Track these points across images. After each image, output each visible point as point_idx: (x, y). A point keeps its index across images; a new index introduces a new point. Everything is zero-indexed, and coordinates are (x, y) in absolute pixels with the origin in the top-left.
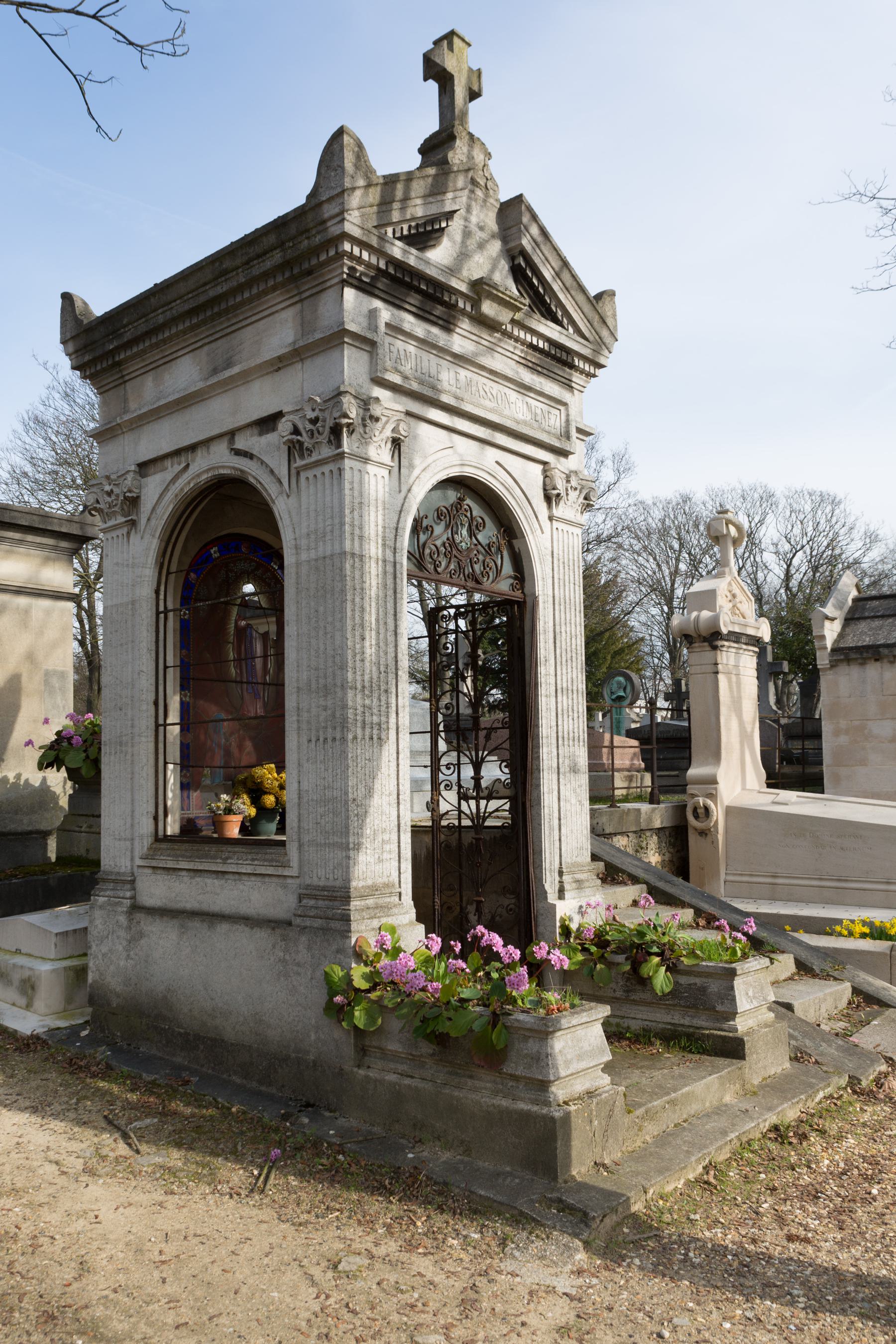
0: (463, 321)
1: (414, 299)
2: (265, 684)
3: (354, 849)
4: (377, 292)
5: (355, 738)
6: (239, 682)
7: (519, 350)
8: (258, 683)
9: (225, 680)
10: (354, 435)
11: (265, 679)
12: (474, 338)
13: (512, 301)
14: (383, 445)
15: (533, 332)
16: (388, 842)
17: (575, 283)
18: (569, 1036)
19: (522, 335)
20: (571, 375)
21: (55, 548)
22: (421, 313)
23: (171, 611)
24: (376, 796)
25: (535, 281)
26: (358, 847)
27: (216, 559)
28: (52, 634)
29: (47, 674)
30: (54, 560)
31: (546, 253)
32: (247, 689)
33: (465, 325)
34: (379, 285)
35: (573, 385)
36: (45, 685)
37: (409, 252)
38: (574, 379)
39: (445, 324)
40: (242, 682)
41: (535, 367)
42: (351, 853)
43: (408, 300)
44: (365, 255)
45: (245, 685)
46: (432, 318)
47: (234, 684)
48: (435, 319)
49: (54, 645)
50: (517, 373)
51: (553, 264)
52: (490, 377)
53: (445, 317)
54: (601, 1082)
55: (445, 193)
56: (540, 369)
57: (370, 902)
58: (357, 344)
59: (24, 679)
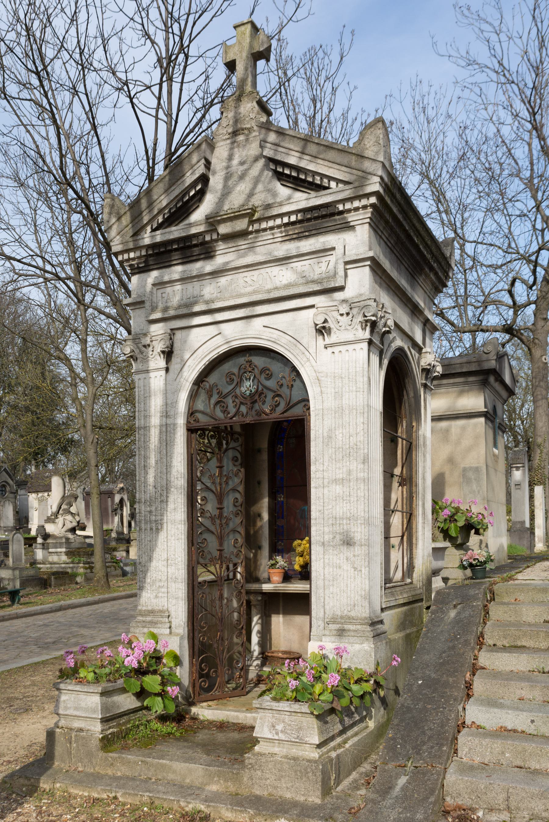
1: (176, 256)
4: (151, 267)
7: (278, 233)
12: (233, 249)
15: (281, 216)
16: (162, 587)
17: (322, 148)
20: (345, 218)
21: (466, 383)
22: (185, 260)
24: (154, 561)
25: (287, 172)
28: (466, 442)
29: (465, 470)
30: (468, 391)
31: (286, 145)
33: (221, 246)
34: (151, 263)
35: (352, 224)
36: (463, 478)
38: (349, 220)
39: (207, 255)
41: (301, 235)
44: (132, 255)
46: (195, 258)
49: (469, 449)
50: (538, 159)
51: (296, 149)
54: (93, 728)
55: (184, 176)
56: (307, 234)
57: (149, 619)
58: (138, 307)
59: (447, 476)
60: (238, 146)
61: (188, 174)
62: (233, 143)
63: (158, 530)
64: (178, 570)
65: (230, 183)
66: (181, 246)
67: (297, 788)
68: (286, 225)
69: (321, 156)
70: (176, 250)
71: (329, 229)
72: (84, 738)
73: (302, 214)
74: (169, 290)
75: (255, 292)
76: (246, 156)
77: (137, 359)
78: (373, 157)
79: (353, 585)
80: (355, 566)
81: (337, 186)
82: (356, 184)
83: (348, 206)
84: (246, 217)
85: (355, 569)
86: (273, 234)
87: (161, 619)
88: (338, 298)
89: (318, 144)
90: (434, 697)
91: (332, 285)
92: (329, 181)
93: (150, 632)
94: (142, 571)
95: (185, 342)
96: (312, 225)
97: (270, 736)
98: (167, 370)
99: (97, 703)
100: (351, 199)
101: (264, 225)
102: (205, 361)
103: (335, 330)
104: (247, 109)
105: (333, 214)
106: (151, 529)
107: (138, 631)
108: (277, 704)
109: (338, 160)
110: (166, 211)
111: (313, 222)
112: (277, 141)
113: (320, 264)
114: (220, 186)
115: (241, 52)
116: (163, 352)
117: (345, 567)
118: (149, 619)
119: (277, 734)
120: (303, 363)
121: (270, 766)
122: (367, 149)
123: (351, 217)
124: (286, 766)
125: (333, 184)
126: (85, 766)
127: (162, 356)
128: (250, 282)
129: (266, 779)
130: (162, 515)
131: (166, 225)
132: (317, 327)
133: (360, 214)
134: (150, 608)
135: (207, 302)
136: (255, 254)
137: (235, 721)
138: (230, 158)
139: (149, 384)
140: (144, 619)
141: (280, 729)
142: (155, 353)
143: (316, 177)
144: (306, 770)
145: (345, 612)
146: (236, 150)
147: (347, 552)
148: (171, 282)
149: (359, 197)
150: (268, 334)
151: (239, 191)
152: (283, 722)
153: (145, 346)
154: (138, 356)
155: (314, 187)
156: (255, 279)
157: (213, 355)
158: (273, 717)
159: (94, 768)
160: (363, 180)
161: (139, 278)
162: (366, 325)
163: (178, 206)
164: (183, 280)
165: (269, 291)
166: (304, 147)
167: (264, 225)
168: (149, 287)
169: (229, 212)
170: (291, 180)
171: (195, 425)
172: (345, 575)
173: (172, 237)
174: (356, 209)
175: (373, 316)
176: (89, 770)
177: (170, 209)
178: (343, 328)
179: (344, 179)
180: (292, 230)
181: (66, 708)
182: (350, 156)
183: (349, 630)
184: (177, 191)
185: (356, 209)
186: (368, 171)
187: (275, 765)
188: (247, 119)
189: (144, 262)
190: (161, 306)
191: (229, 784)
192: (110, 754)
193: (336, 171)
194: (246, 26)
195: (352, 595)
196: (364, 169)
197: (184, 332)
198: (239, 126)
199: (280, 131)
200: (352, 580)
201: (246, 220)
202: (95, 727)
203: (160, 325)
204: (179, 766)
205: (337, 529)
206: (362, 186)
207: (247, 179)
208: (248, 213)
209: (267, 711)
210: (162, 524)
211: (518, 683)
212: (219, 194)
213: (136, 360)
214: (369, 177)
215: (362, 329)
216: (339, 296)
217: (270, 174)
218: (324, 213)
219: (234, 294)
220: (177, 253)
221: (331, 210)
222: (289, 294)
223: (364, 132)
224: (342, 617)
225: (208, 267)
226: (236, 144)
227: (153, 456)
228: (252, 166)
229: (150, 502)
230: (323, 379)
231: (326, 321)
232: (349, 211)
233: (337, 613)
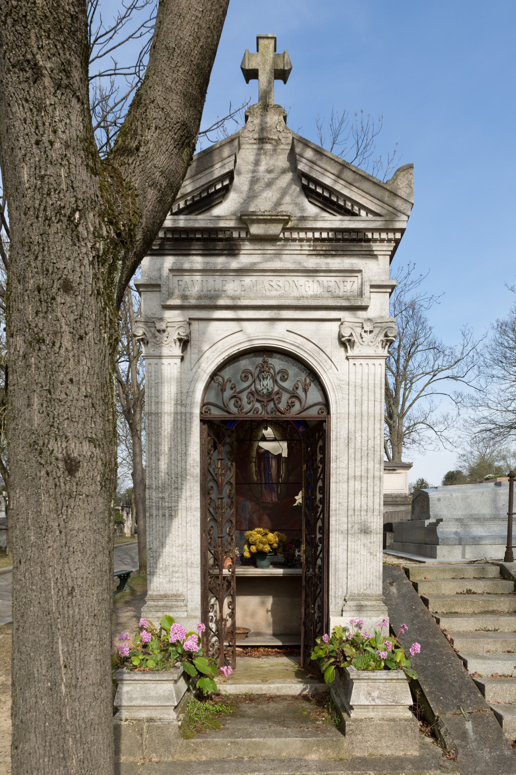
0: (244, 245)
1: (197, 245)
2: (278, 483)
3: (150, 575)
4: (167, 252)
5: (151, 515)
7: (306, 246)
8: (273, 483)
10: (149, 345)
11: (278, 480)
12: (259, 252)
13: (273, 217)
14: (173, 345)
15: (313, 230)
17: (358, 177)
18: (138, 685)
19: (302, 235)
20: (370, 246)
22: (206, 252)
25: (319, 190)
26: (153, 574)
31: (323, 165)
33: (247, 246)
34: (167, 247)
35: (375, 253)
37: (178, 220)
38: (374, 249)
39: (230, 252)
40: (261, 484)
41: (328, 253)
42: (148, 577)
43: (192, 248)
46: (217, 252)
47: (256, 485)
48: (220, 252)
51: (332, 171)
52: (275, 274)
53: (228, 248)
54: (166, 716)
55: (212, 166)
56: (334, 253)
57: (161, 603)
58: (150, 290)
60: (265, 154)
61: (217, 166)
62: (260, 149)
63: (171, 517)
64: (194, 555)
65: (256, 187)
66: (205, 236)
67: (396, 745)
68: (316, 240)
69: (356, 184)
70: (198, 240)
71: (354, 253)
72: (159, 727)
73: (333, 233)
74: (187, 278)
75: (280, 297)
76: (274, 165)
77: (148, 343)
78: (405, 198)
79: (369, 568)
80: (371, 551)
81: (367, 215)
82: (387, 218)
83: (376, 236)
84: (281, 223)
85: (371, 554)
86: (301, 246)
87: (176, 603)
88: (361, 317)
89: (354, 172)
90: (435, 655)
91: (359, 303)
92: (359, 210)
93: (166, 616)
94: (153, 557)
95: (204, 333)
96: (340, 246)
97: (367, 703)
98: (182, 359)
99: (171, 691)
100: (379, 230)
101: (295, 235)
102: (225, 355)
103: (358, 344)
104: (273, 120)
105: (361, 240)
106: (164, 515)
107: (150, 616)
108: (374, 674)
109: (373, 192)
110: (189, 198)
111: (341, 243)
112: (314, 159)
113: (345, 283)
114: (245, 188)
115: (264, 64)
116: (180, 340)
117: (362, 553)
118: (161, 603)
119: (374, 700)
120: (326, 370)
121: (370, 730)
122: (400, 189)
123: (376, 247)
124: (386, 728)
125: (363, 213)
126: (161, 756)
127: (178, 343)
128: (275, 287)
129: (366, 742)
130: (177, 502)
131: (186, 212)
132: (343, 339)
133: (384, 246)
134: (162, 593)
135: (233, 298)
136: (281, 260)
137: (259, 693)
138: (257, 163)
139: (161, 370)
140: (156, 603)
141: (376, 696)
142: (169, 340)
143: (347, 203)
144: (405, 728)
145: (362, 591)
146: (263, 157)
147: (364, 539)
148: (191, 271)
149: (387, 230)
150: (291, 338)
151: (266, 198)
152: (379, 689)
153: (159, 331)
154: (150, 340)
155: (342, 212)
156: (281, 284)
157: (234, 350)
158: (368, 685)
159: (173, 756)
160: (393, 216)
161: (151, 261)
162: (386, 344)
163: (203, 196)
164: (204, 271)
165: (298, 298)
166: (341, 172)
167: (295, 235)
168: (165, 272)
169: (266, 213)
170: (321, 200)
171: (207, 416)
172: (362, 559)
173: (197, 225)
174: (382, 241)
175: (394, 337)
176: (166, 759)
177: (193, 198)
178: (366, 343)
179: (375, 211)
180: (320, 247)
181: (131, 699)
182: (384, 191)
183: (366, 606)
184: (203, 181)
185: (382, 241)
186: (398, 209)
187: (376, 728)
188: (274, 130)
189: (159, 245)
190: (177, 292)
191: (329, 751)
192: (193, 740)
193: (368, 201)
194: (270, 40)
195: (368, 576)
196: (396, 206)
197: (202, 324)
198: (265, 135)
199: (318, 149)
200: (368, 563)
201: (280, 226)
202: (169, 715)
203: (177, 312)
204: (274, 742)
205: (357, 519)
206: (392, 221)
207: (274, 188)
208: (285, 220)
209: (362, 681)
210: (176, 511)
211: (485, 640)
212: (244, 195)
213: (146, 343)
214: (399, 214)
215: (382, 347)
216: (361, 314)
217: (298, 189)
218: (354, 237)
219: (260, 295)
220: (199, 243)
221: (361, 236)
222: (318, 304)
223: (397, 173)
224: (359, 595)
225: (234, 264)
226: (262, 151)
227: (166, 443)
228: (279, 176)
229: (163, 488)
230: (344, 386)
231: (351, 335)
232: (375, 240)
233: (354, 591)
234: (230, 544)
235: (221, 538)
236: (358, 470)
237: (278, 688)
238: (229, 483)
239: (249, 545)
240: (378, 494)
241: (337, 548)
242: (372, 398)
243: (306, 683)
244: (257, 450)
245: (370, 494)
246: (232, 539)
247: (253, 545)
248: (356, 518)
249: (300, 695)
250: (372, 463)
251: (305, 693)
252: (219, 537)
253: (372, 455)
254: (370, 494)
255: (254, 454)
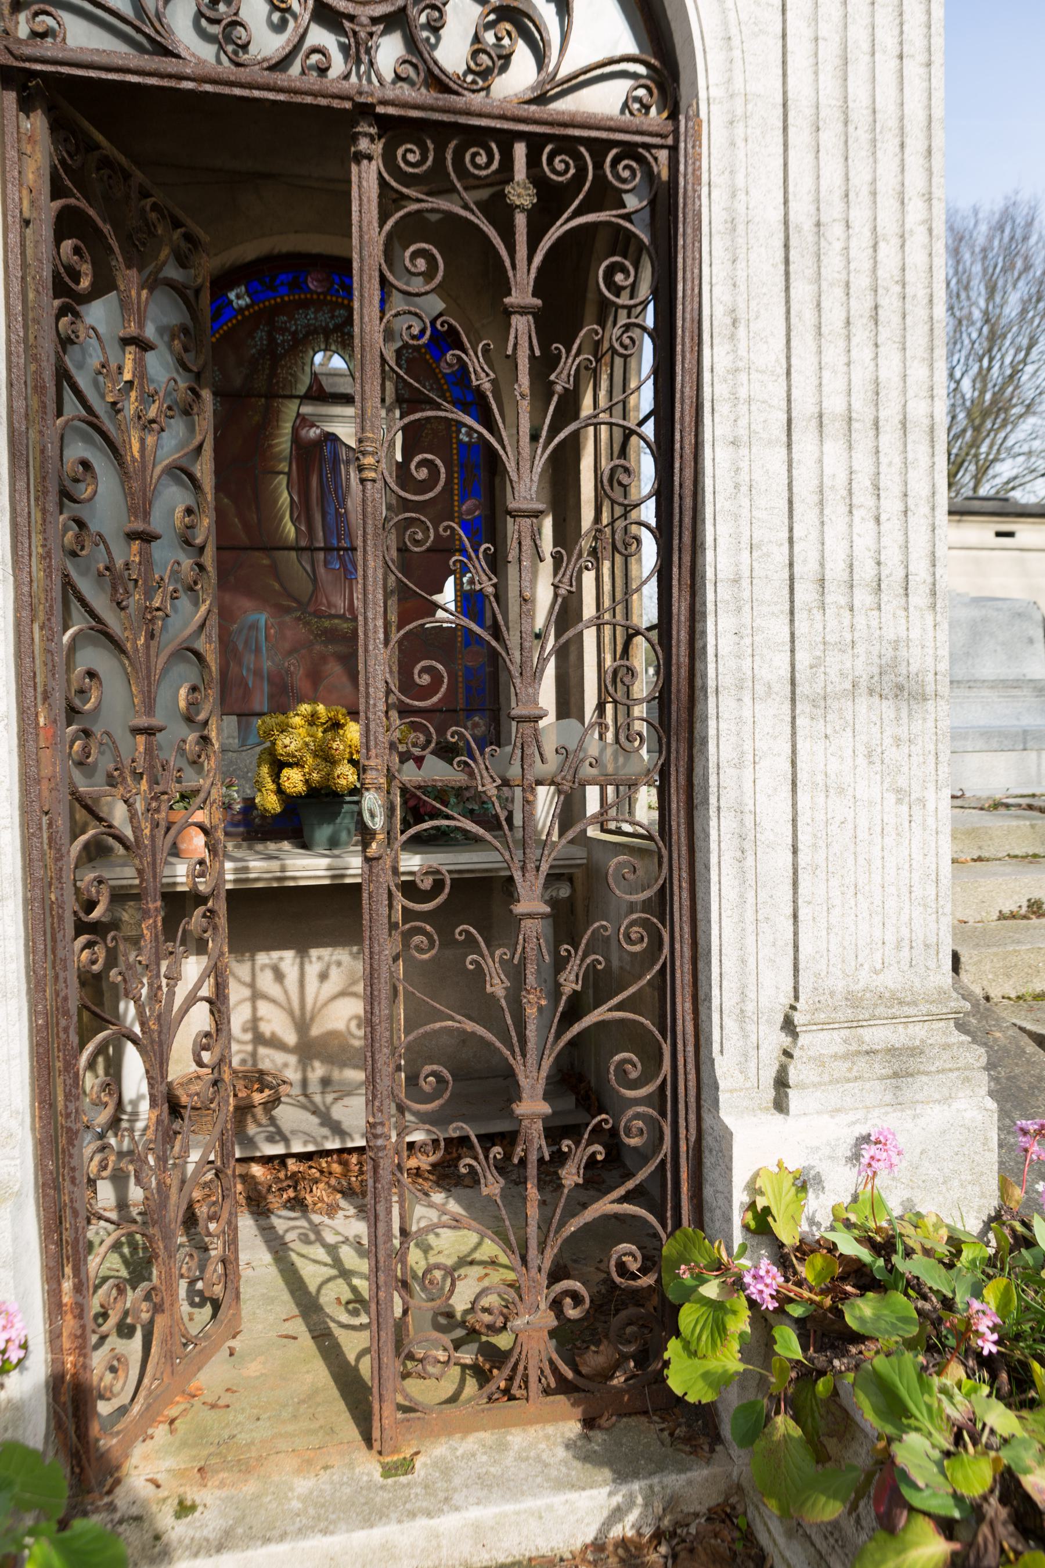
6: (303, 549)
9: (275, 546)
23: (285, 459)
27: (241, 310)
32: (326, 563)
40: (311, 549)
45: (321, 555)
80: (902, 782)
85: (901, 794)
145: (865, 977)
200: (889, 841)
224: (853, 1000)
234: (195, 763)
235: (149, 732)
236: (834, 384)
237: (477, 1527)
238: (182, 473)
239: (278, 765)
240: (925, 509)
241: (748, 774)
242: (887, 39)
243: (622, 1476)
244: (295, 431)
245: (891, 506)
246: (205, 740)
247: (290, 765)
248: (832, 623)
249: (598, 1546)
250: (896, 358)
251: (616, 1532)
252: (136, 731)
253: (896, 319)
254: (891, 506)
255: (283, 442)
